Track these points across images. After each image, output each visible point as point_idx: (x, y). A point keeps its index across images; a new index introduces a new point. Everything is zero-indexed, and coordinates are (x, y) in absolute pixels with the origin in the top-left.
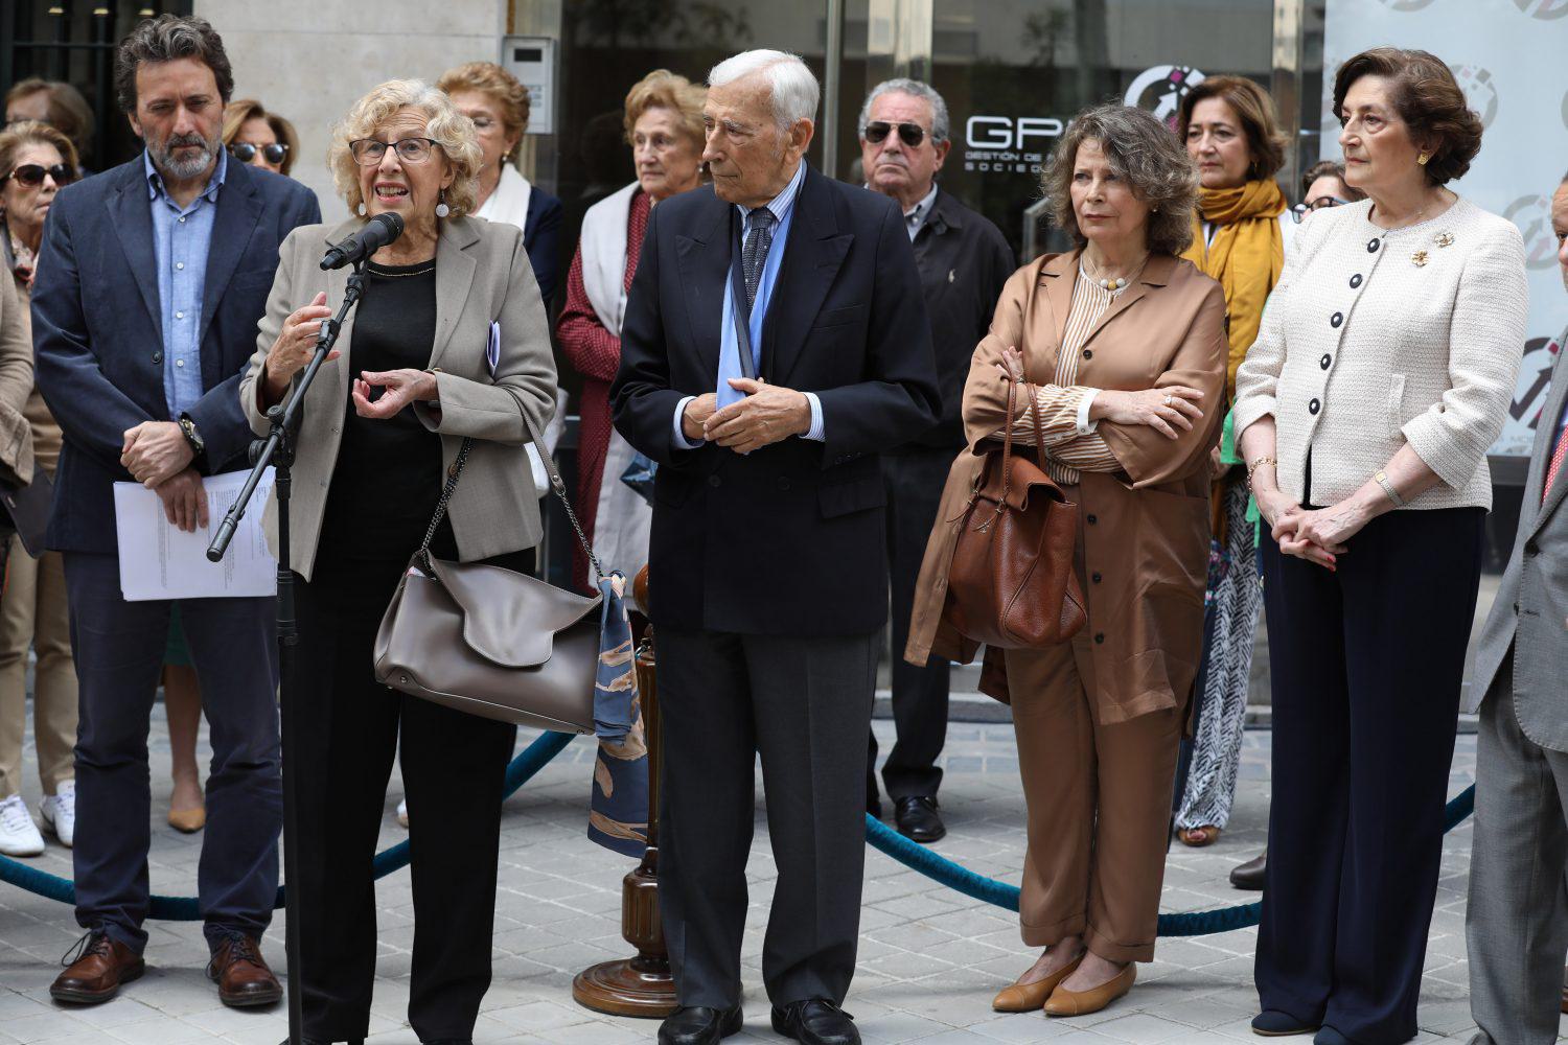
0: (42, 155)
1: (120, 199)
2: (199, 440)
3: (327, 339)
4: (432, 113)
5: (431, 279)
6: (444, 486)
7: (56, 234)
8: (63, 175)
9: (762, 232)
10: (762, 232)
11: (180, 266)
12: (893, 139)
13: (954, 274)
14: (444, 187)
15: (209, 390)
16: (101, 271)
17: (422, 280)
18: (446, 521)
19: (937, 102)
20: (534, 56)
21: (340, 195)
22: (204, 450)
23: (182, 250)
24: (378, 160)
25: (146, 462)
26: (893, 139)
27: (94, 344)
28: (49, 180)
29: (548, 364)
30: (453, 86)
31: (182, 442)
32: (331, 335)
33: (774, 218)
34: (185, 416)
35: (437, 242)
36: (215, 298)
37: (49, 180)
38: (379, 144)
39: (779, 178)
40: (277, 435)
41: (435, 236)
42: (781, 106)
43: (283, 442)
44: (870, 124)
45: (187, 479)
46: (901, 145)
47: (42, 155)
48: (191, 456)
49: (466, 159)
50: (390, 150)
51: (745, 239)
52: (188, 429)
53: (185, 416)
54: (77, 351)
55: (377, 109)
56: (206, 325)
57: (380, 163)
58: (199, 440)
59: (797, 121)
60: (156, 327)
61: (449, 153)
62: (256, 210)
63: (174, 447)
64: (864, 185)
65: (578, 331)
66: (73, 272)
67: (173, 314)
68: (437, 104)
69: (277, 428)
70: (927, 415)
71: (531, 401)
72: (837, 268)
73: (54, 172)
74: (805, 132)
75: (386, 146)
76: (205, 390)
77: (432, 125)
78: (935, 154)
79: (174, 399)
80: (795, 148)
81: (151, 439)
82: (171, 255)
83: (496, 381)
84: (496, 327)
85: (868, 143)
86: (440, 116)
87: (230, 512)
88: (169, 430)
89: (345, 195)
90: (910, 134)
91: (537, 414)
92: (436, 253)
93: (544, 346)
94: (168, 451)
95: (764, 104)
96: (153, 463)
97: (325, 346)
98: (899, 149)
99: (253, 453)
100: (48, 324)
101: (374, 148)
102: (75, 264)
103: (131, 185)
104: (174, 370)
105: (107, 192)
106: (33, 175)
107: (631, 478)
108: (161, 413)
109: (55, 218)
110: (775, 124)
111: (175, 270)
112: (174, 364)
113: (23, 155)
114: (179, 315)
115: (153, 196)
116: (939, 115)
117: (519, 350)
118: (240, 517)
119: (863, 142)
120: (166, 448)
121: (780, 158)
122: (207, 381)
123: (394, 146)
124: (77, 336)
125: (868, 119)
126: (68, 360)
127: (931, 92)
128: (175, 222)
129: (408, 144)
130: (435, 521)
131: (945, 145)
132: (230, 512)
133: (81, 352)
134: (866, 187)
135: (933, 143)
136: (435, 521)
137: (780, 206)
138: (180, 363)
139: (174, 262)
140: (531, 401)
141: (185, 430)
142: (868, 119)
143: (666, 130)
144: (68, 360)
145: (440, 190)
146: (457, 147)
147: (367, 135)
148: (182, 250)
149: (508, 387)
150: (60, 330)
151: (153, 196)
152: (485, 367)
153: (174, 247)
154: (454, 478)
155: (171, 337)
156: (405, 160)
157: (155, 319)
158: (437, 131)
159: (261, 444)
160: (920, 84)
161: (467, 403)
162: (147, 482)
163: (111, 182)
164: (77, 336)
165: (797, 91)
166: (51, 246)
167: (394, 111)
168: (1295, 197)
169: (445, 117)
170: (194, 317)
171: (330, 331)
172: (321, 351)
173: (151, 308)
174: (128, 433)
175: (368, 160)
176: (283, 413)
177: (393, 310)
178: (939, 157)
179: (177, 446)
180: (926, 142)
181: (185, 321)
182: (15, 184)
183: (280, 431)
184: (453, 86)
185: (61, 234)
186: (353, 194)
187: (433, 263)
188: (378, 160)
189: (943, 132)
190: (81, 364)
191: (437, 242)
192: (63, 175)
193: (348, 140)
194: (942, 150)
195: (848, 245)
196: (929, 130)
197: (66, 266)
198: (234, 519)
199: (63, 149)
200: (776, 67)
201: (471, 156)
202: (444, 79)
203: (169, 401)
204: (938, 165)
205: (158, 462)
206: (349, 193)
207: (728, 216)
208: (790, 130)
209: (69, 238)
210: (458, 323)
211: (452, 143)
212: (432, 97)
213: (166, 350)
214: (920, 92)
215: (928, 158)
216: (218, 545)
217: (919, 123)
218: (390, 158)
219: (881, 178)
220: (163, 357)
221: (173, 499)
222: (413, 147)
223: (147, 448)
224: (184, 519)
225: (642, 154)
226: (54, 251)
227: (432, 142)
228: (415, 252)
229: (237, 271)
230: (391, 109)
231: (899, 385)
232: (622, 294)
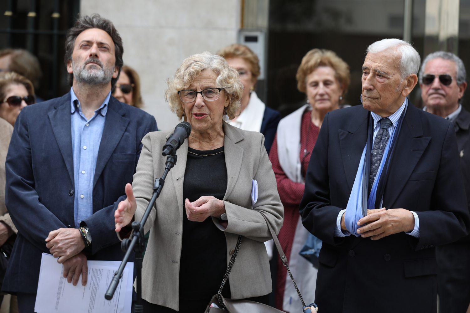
0: (18, 90)
1: (56, 113)
2: (89, 239)
3: (158, 188)
4: (217, 72)
5: (223, 156)
6: (228, 266)
7: (21, 128)
8: (29, 100)
9: (385, 130)
10: (385, 130)
11: (85, 147)
12: (436, 83)
13: (463, 152)
14: (226, 106)
15: (95, 212)
16: (43, 148)
17: (219, 156)
18: (227, 283)
19: (459, 62)
20: (254, 39)
21: (173, 111)
22: (91, 245)
23: (87, 138)
24: (193, 100)
25: (59, 248)
26: (436, 83)
27: (36, 186)
28: (24, 104)
29: (278, 201)
30: (228, 56)
31: (80, 239)
32: (160, 186)
33: (391, 124)
34: (83, 224)
35: (224, 137)
36: (102, 165)
37: (24, 104)
38: (194, 93)
39: (396, 103)
40: (137, 236)
41: (222, 134)
42: (405, 66)
43: (140, 240)
44: (425, 75)
45: (79, 259)
46: (441, 85)
47: (18, 90)
48: (84, 246)
49: (236, 92)
50: (199, 95)
51: (375, 134)
52: (83, 233)
53: (83, 224)
54: (26, 188)
55: (190, 73)
56: (97, 178)
57: (195, 101)
58: (89, 239)
59: (411, 75)
60: (71, 177)
61: (227, 90)
62: (126, 121)
63: (75, 242)
64: (422, 108)
65: (285, 183)
66: (27, 148)
67: (80, 171)
68: (220, 67)
69: (136, 232)
70: (464, 230)
71: (272, 218)
72: (422, 152)
73: (24, 99)
74: (413, 81)
75: (197, 93)
76: (94, 211)
77: (220, 77)
78: (459, 90)
79: (77, 214)
80: (408, 88)
81: (64, 236)
82: (81, 142)
83: (255, 209)
84: (255, 182)
85: (424, 85)
86: (222, 74)
87: (116, 275)
88: (73, 233)
89: (176, 112)
90: (445, 80)
91: (275, 225)
92: (224, 144)
93: (275, 193)
94: (72, 243)
95: (397, 64)
96: (63, 249)
97: (158, 191)
98: (440, 87)
99: (124, 245)
100: (14, 173)
101: (191, 94)
102: (29, 144)
103: (61, 106)
104: (78, 199)
105: (49, 109)
106: (15, 101)
107: (304, 253)
108: (69, 223)
109: (21, 121)
110: (401, 74)
111: (82, 150)
112: (79, 197)
113: (9, 91)
114: (83, 172)
115: (73, 111)
116: (461, 69)
117: (264, 194)
118: (120, 277)
119: (422, 85)
120: (71, 242)
121: (400, 92)
122: (95, 208)
123: (201, 93)
124: (28, 182)
125: (423, 73)
126: (23, 193)
127: (456, 58)
128: (84, 126)
129: (207, 91)
130: (223, 284)
131: (464, 85)
132: (116, 275)
133: (29, 190)
134: (424, 110)
135: (458, 84)
136: (223, 284)
137: (395, 118)
138: (82, 196)
139: (82, 146)
140: (272, 218)
141: (82, 233)
142: (423, 73)
143: (331, 78)
144: (23, 193)
145: (225, 108)
146: (232, 87)
147: (186, 87)
148: (87, 138)
149: (261, 211)
150: (20, 177)
151: (73, 111)
152: (250, 200)
153: (82, 138)
154: (233, 259)
155: (78, 183)
156: (207, 99)
157: (70, 173)
158: (221, 81)
159: (128, 241)
160: (450, 54)
161: (239, 218)
162: (61, 258)
163: (51, 105)
164: (28, 182)
165: (412, 60)
166: (17, 135)
167: (197, 75)
168: (238, 100)
169: (225, 73)
170: (91, 173)
171: (160, 184)
172: (155, 194)
173: (68, 167)
174: (52, 233)
175: (188, 101)
176: (140, 225)
177: (207, 172)
178: (461, 91)
179: (77, 241)
180: (454, 83)
181: (86, 175)
182: (6, 105)
183: (138, 234)
184: (228, 56)
185: (23, 129)
186: (179, 111)
187: (222, 149)
188: (193, 100)
189: (462, 78)
190: (31, 196)
191: (224, 137)
192: (29, 100)
193: (177, 90)
194: (462, 87)
195: (428, 142)
196: (455, 77)
197: (24, 145)
198: (118, 278)
199: (28, 88)
200: (403, 47)
201: (238, 90)
202: (222, 52)
203: (75, 216)
204: (461, 95)
205: (67, 249)
206: (177, 110)
207: (366, 121)
208: (407, 79)
209: (27, 131)
210: (237, 179)
211: (229, 85)
212: (216, 62)
213: (75, 189)
214: (450, 58)
215: (455, 91)
216: (110, 291)
217: (449, 73)
218: (199, 99)
219: (431, 102)
220: (74, 192)
221: (70, 268)
222: (210, 92)
223: (62, 240)
224: (71, 278)
225: (311, 91)
226: (19, 138)
227: (220, 90)
228: (213, 141)
229: (114, 152)
230: (197, 73)
231: (452, 213)
232: (298, 163)
